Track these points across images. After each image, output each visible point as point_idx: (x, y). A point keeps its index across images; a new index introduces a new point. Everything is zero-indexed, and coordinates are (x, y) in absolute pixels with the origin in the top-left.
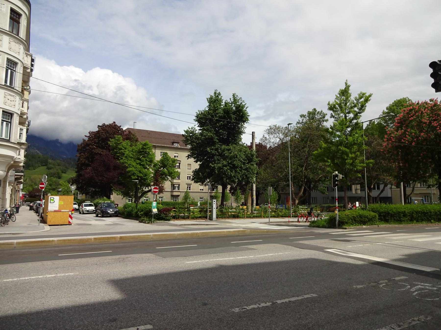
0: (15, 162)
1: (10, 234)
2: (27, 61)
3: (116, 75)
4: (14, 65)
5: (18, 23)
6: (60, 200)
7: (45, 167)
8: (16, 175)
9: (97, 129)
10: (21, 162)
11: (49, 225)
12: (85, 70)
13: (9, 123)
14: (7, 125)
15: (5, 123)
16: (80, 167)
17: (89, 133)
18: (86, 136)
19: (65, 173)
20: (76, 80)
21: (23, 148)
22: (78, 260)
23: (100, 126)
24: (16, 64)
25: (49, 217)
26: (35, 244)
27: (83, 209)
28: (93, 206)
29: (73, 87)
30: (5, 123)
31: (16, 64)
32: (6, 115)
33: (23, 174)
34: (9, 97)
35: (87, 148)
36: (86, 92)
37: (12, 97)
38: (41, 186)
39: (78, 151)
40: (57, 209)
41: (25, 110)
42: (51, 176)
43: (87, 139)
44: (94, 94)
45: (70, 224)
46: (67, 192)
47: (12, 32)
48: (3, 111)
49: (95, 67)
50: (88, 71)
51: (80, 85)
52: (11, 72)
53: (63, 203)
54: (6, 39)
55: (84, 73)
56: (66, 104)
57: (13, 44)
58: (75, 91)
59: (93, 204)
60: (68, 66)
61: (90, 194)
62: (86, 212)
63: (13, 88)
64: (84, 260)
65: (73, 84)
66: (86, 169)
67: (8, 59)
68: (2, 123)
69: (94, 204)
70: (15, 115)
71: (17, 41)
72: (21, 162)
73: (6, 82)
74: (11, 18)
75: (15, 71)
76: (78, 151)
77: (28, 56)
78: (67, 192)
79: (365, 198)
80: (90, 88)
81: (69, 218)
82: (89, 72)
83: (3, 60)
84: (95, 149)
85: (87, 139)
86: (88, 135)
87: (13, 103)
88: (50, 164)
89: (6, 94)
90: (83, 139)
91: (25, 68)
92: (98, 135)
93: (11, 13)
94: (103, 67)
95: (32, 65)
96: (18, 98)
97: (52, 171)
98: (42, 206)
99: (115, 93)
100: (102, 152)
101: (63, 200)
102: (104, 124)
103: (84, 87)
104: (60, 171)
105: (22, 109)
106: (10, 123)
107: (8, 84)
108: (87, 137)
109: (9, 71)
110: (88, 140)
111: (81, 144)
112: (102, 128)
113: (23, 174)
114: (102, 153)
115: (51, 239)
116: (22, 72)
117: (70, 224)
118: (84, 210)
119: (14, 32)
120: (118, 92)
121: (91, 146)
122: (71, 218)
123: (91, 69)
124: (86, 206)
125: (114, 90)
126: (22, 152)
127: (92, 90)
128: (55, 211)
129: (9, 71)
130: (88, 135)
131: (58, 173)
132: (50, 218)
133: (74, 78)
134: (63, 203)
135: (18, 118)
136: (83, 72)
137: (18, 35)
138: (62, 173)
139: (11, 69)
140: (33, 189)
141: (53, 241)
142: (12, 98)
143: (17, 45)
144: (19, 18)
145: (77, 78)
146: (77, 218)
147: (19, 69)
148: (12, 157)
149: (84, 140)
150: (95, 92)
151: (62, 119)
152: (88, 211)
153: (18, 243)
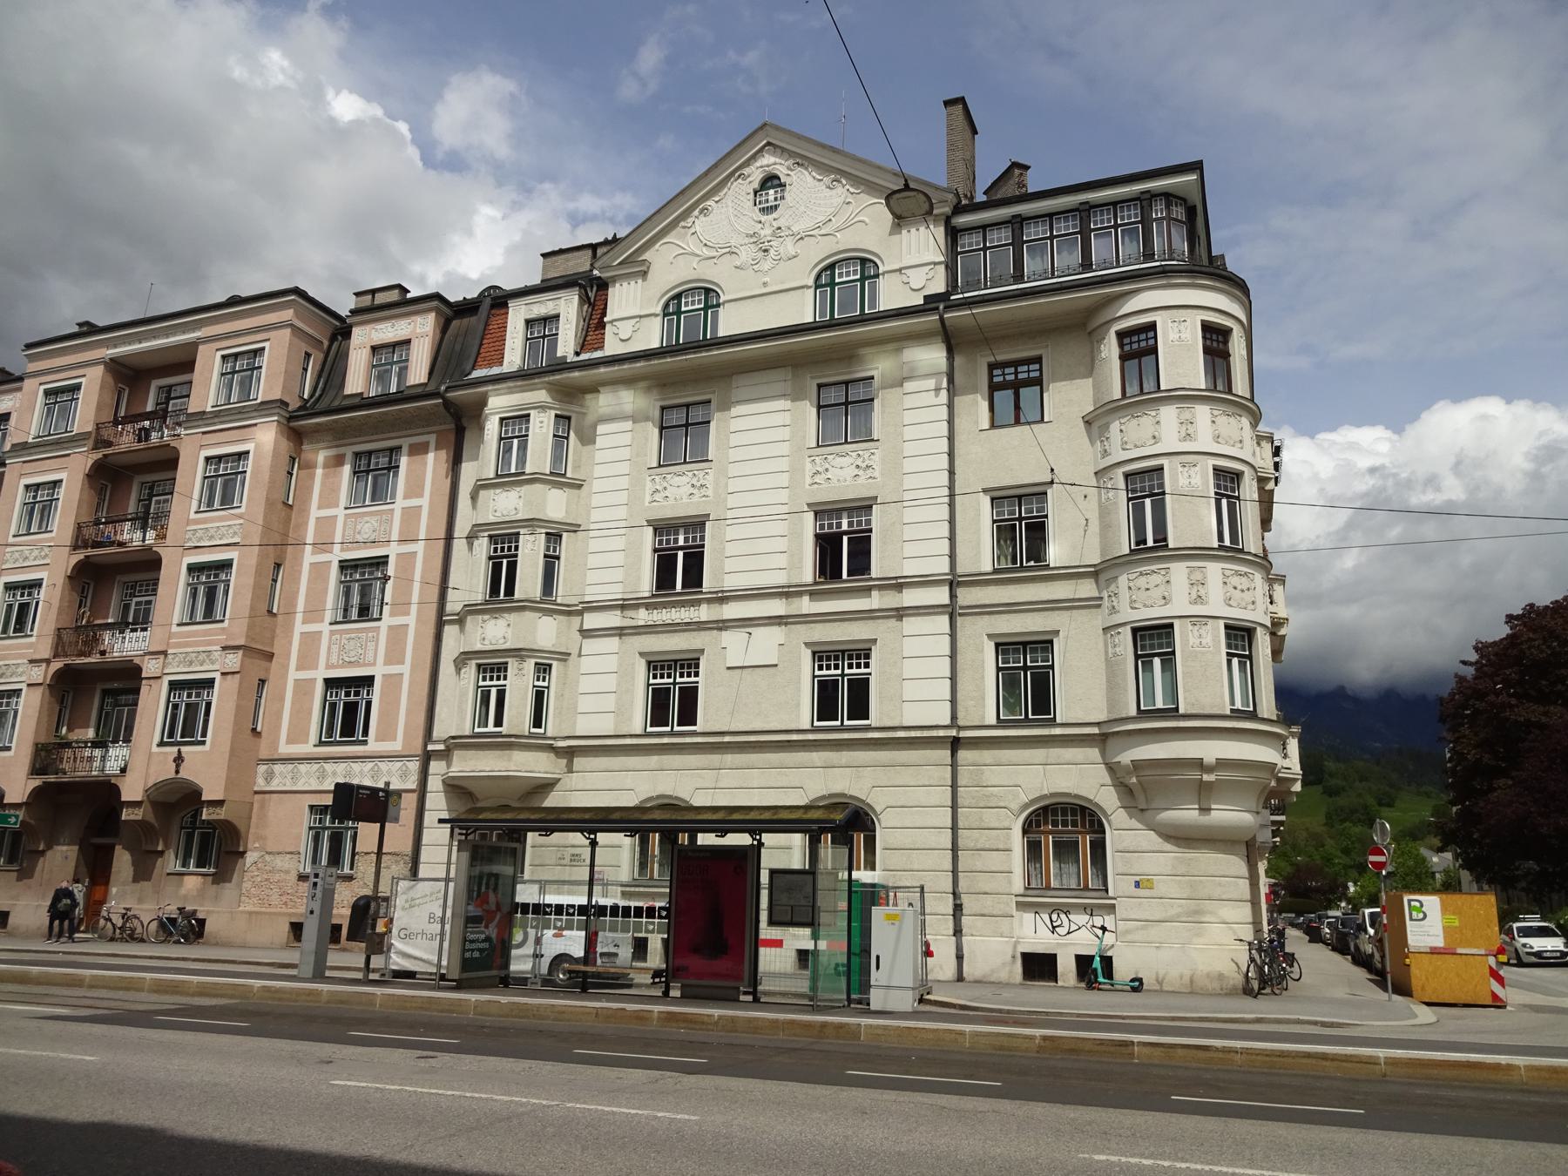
0: (1280, 780)
1: (1315, 1023)
2: (1264, 460)
3: (1521, 407)
4: (1232, 480)
5: (1226, 355)
6: (1445, 909)
7: (1319, 788)
8: (1274, 823)
9: (1504, 631)
10: (1295, 780)
11: (1428, 1004)
12: (1397, 426)
13: (1247, 659)
14: (1242, 665)
15: (1235, 661)
16: (1467, 783)
17: (1476, 649)
18: (1464, 663)
19: (1390, 805)
20: (1372, 470)
21: (1293, 735)
22: (890, 1095)
23: (1517, 617)
24: (1237, 476)
25: (1414, 971)
26: (1448, 1073)
27: (1518, 946)
28: (1556, 935)
29: (1366, 495)
30: (1235, 661)
31: (1237, 476)
32: (1151, 637)
33: (1283, 818)
34: (1235, 580)
35: (1480, 705)
36: (1418, 499)
37: (1244, 579)
38: (1373, 858)
39: (1442, 720)
40: (1439, 942)
41: (1281, 611)
42: (1343, 821)
43: (1470, 672)
44: (1450, 502)
45: (1498, 1003)
46: (1418, 877)
47: (1215, 390)
48: (1227, 627)
49: (1428, 406)
50: (1408, 427)
51: (1390, 482)
52: (1229, 504)
53: (1457, 923)
54: (1203, 412)
55: (1395, 437)
56: (1349, 561)
57: (1222, 420)
58: (1379, 505)
59: (1552, 926)
60: (1333, 429)
61: (1524, 884)
62: (1534, 959)
63: (1241, 551)
64: (1281, 1130)
65: (1364, 485)
66: (1492, 789)
67: (1216, 469)
68: (1229, 662)
69: (1559, 926)
70: (1259, 630)
71: (1230, 410)
72: (1295, 780)
73: (1221, 538)
74: (1207, 350)
75: (1238, 498)
76: (1442, 720)
77: (1264, 443)
78: (1418, 877)
79: (1052, 722)
80: (1432, 481)
81: (1493, 981)
82: (1412, 431)
83: (1204, 476)
84: (1511, 706)
85: (1470, 672)
86: (1474, 657)
87: (1248, 596)
88: (1331, 775)
89: (1228, 573)
90: (1456, 675)
91: (1262, 481)
92: (1515, 652)
93: (1204, 338)
94: (1460, 394)
95: (1277, 466)
96: (1258, 577)
97: (1342, 801)
98: (1366, 931)
99: (1536, 477)
100: (1546, 714)
101: (1458, 912)
102: (1532, 605)
103: (1408, 484)
104: (1371, 801)
105: (1272, 608)
106: (1250, 657)
107: (1227, 542)
108: (1471, 664)
109: (1224, 502)
110: (1476, 678)
111: (1452, 694)
112: (1525, 624)
113: (1283, 818)
114: (1544, 719)
115: (1503, 1059)
116: (1256, 496)
117: (1498, 1003)
118: (1522, 951)
119: (1220, 388)
120: (1545, 470)
121: (1492, 698)
122: (1501, 980)
123: (1415, 417)
124: (1528, 932)
125: (1528, 466)
126: (1293, 746)
127: (1438, 489)
128: (1434, 951)
129: (1224, 502)
130: (1474, 657)
131: (1365, 807)
132: (1419, 974)
133: (1364, 463)
134: (1457, 923)
135: (1268, 638)
136: (1388, 434)
137: (1230, 391)
138: (1380, 804)
139: (1228, 497)
140: (1297, 867)
141: (1509, 1067)
142: (1243, 583)
143: (1232, 420)
144: (1226, 342)
145: (1377, 462)
146: (1518, 985)
147: (1249, 489)
148: (1271, 767)
149: (1461, 679)
150: (1453, 491)
151: (1348, 613)
152: (1538, 954)
153: (1392, 1062)
